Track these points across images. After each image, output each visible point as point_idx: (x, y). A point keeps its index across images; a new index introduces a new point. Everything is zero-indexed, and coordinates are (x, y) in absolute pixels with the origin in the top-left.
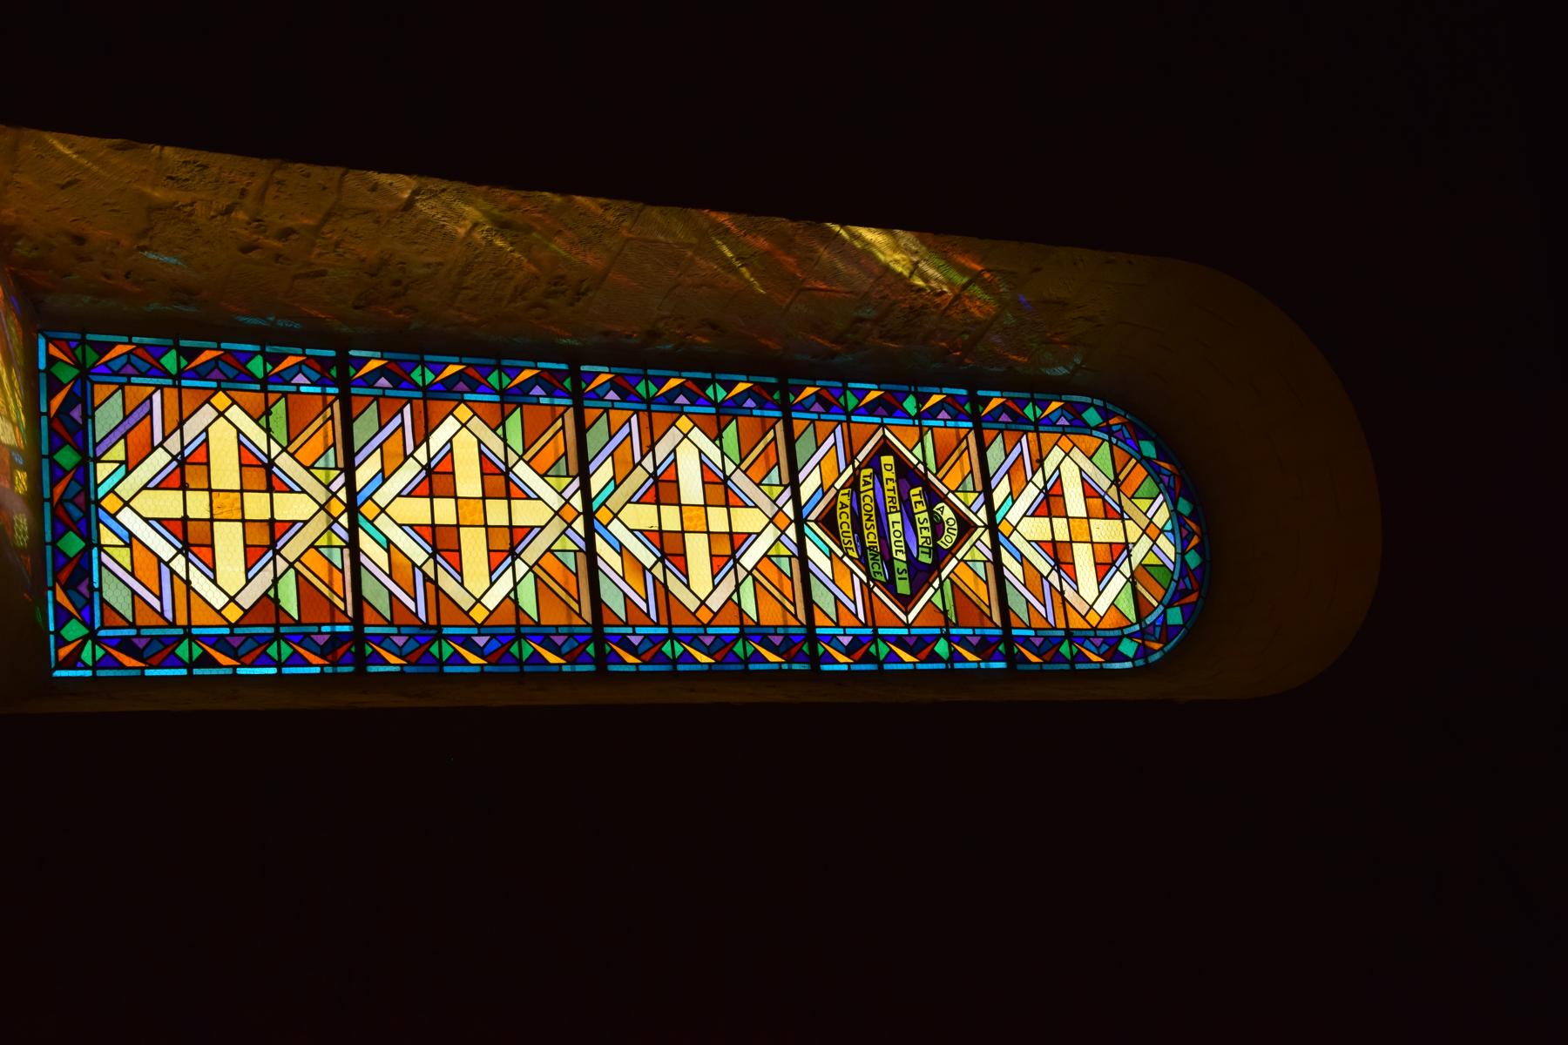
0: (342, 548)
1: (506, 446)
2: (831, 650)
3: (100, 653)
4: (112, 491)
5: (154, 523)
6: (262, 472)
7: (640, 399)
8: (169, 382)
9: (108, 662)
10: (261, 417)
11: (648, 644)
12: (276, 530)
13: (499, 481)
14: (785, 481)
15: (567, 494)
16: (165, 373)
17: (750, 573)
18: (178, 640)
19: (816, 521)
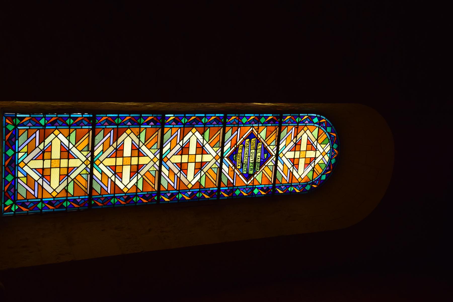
0: (88, 174)
1: (140, 140)
2: (204, 195)
3: (17, 207)
4: (22, 161)
5: (34, 170)
6: (67, 153)
7: (67, 125)
8: (42, 127)
9: (19, 209)
10: (68, 137)
11: (285, 188)
12: (70, 170)
13: (201, 150)
14: (220, 146)
15: (217, 152)
16: (41, 125)
17: (73, 180)
18: (38, 202)
19: (226, 157)
